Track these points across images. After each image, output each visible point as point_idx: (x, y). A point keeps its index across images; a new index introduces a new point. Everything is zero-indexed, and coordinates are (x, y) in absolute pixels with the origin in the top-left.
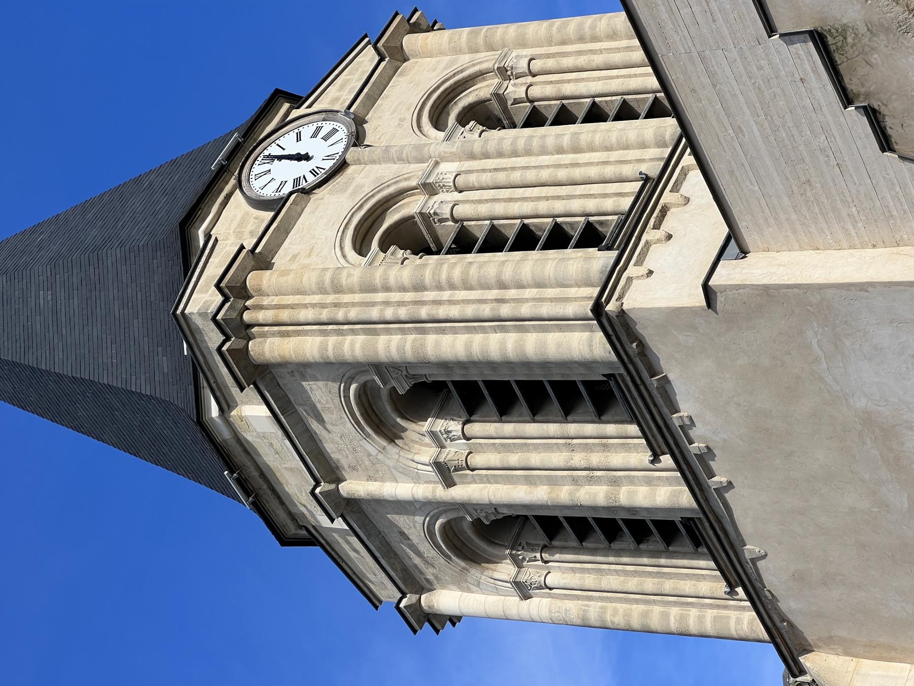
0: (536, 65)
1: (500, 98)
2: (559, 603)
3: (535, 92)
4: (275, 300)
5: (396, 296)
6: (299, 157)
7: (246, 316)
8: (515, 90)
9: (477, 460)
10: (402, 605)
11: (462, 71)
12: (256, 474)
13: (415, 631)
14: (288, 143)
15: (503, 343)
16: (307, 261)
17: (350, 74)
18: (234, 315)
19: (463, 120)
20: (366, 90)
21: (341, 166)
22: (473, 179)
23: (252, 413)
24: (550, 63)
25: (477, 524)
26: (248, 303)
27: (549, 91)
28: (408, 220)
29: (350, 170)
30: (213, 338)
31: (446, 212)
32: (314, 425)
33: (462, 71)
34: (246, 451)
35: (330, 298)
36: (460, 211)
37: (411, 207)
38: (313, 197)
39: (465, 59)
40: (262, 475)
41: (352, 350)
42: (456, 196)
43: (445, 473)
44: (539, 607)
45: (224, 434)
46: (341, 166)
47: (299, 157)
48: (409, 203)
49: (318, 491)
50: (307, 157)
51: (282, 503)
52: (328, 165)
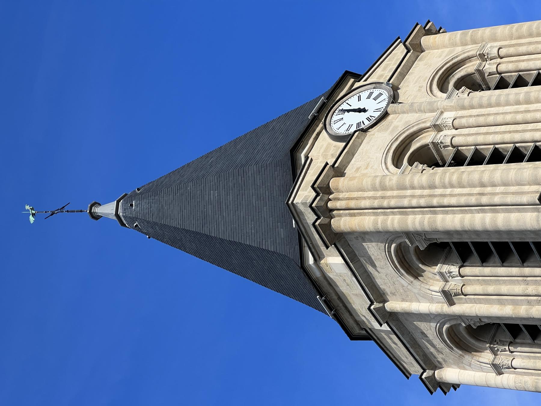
0: (503, 52)
1: (480, 72)
2: (521, 377)
3: (502, 68)
4: (347, 195)
5: (418, 192)
6: (360, 110)
7: (330, 205)
8: (489, 67)
9: (468, 289)
10: (423, 377)
11: (457, 57)
12: (335, 297)
13: (432, 393)
14: (353, 102)
15: (483, 219)
16: (365, 172)
17: (389, 61)
18: (322, 204)
19: (457, 86)
20: (399, 70)
21: (385, 115)
22: (464, 121)
23: (333, 262)
24: (512, 50)
25: (469, 328)
26: (331, 197)
27: (511, 67)
28: (425, 147)
29: (390, 118)
30: (310, 217)
31: (448, 141)
32: (370, 269)
33: (457, 57)
34: (330, 284)
35: (379, 194)
36: (456, 141)
37: (426, 139)
38: (368, 134)
39: (459, 49)
40: (339, 298)
41: (393, 224)
42: (454, 132)
43: (449, 297)
44: (507, 379)
45: (317, 274)
46: (385, 115)
47: (360, 110)
48: (425, 137)
49: (372, 307)
50: (364, 110)
51: (351, 314)
52: (377, 114)
